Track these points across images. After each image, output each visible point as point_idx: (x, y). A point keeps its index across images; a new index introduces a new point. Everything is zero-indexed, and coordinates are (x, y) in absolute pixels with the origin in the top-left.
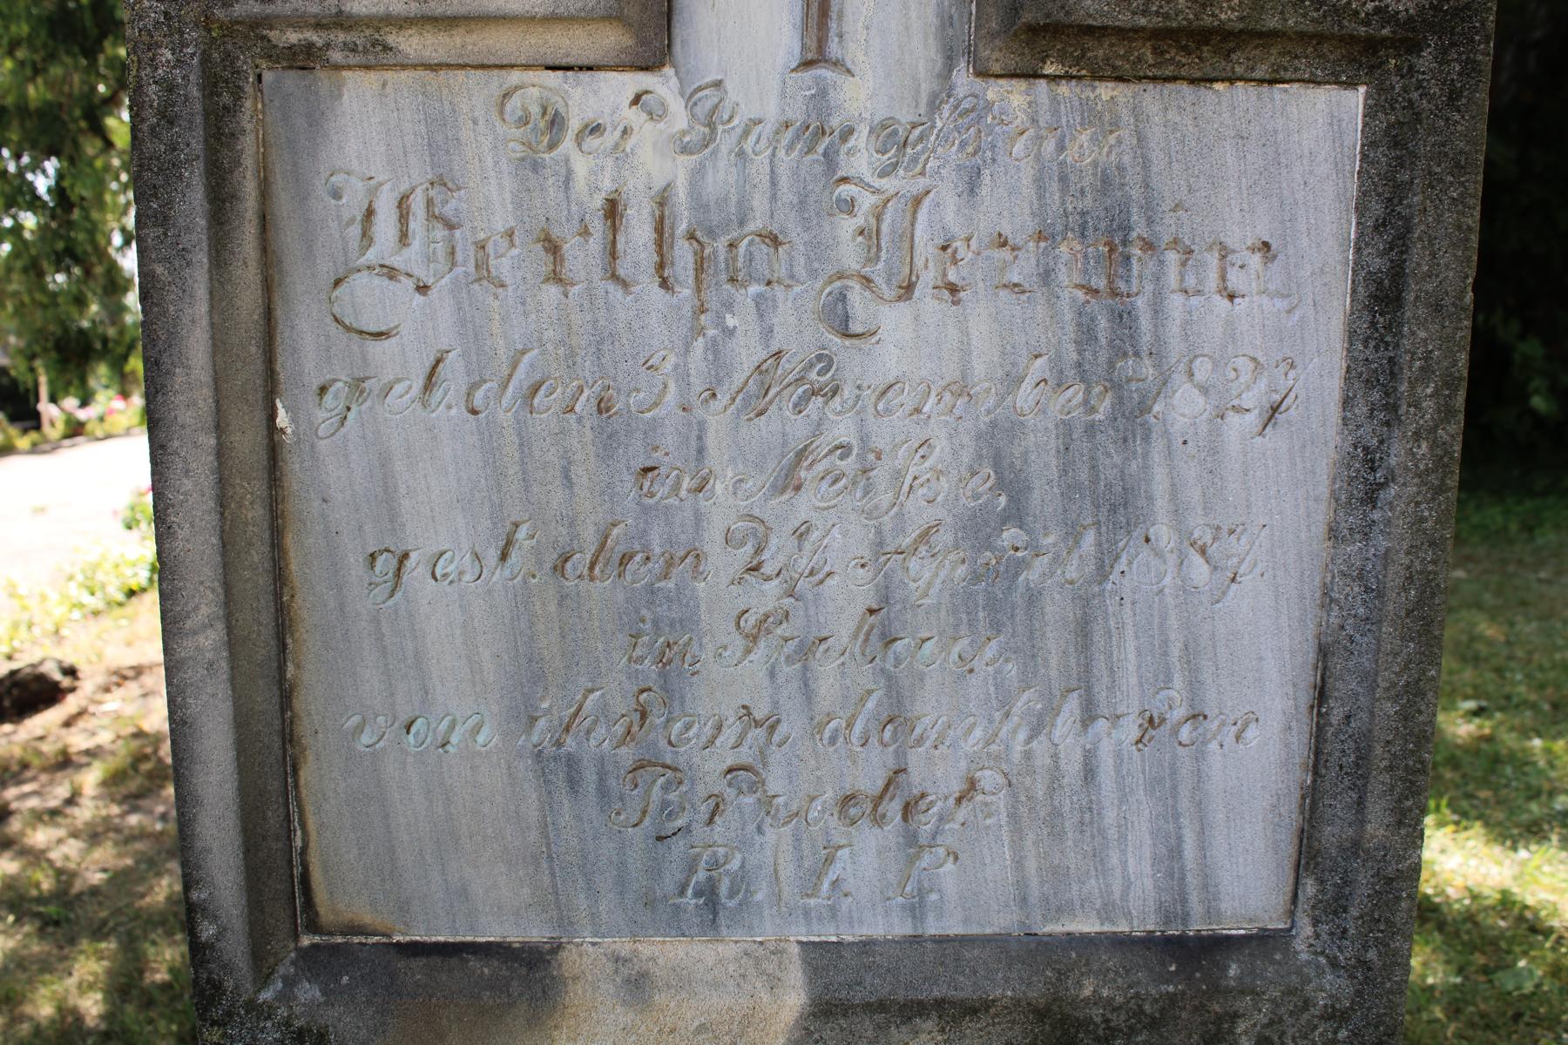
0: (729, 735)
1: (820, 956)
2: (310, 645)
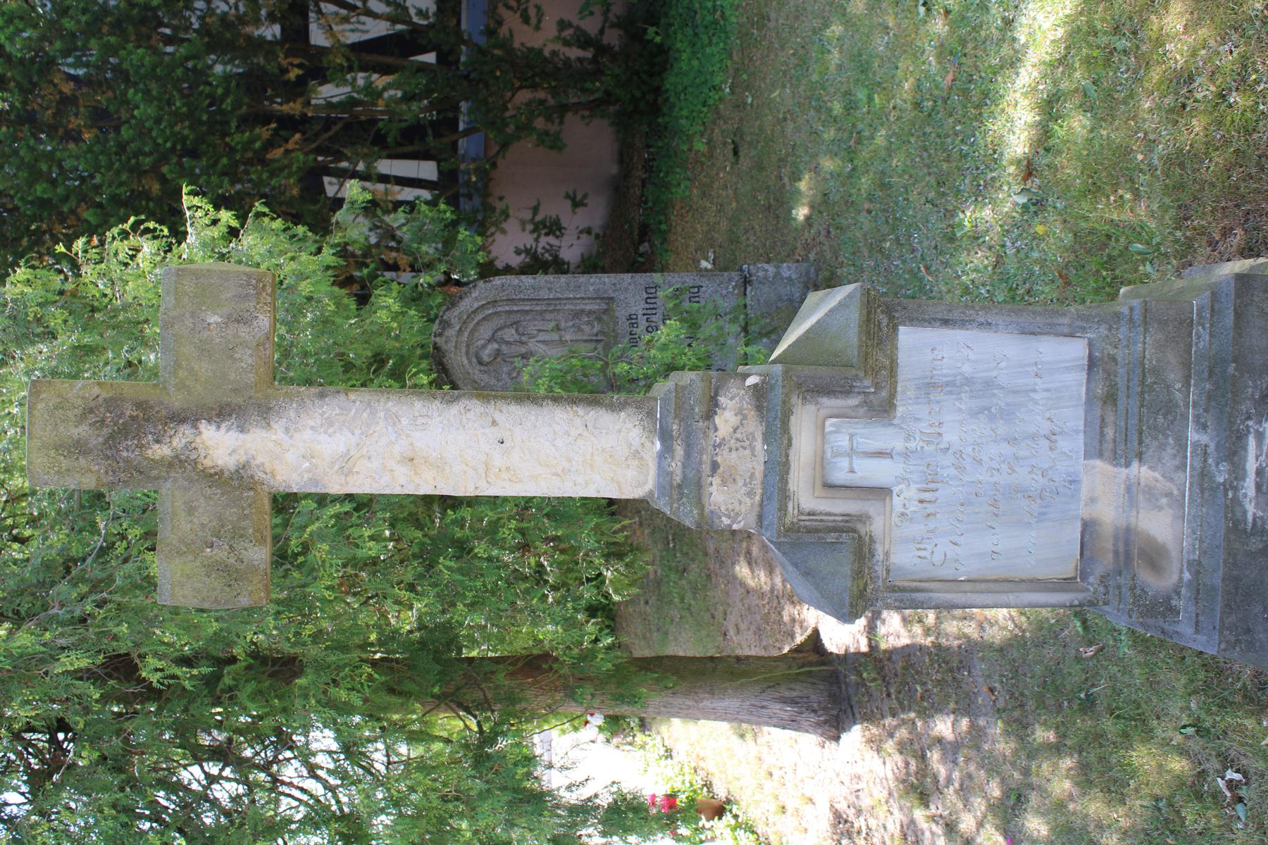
0: (1035, 477)
1: (1087, 456)
2: (1010, 575)
